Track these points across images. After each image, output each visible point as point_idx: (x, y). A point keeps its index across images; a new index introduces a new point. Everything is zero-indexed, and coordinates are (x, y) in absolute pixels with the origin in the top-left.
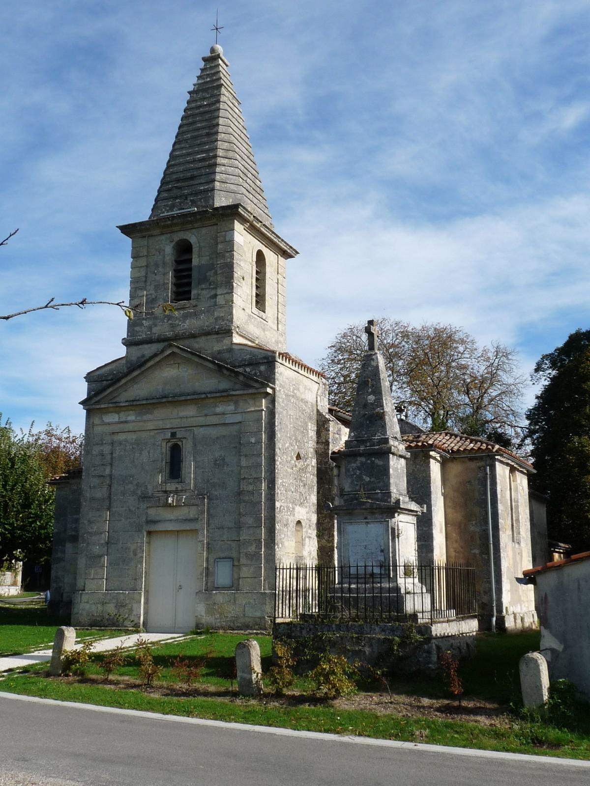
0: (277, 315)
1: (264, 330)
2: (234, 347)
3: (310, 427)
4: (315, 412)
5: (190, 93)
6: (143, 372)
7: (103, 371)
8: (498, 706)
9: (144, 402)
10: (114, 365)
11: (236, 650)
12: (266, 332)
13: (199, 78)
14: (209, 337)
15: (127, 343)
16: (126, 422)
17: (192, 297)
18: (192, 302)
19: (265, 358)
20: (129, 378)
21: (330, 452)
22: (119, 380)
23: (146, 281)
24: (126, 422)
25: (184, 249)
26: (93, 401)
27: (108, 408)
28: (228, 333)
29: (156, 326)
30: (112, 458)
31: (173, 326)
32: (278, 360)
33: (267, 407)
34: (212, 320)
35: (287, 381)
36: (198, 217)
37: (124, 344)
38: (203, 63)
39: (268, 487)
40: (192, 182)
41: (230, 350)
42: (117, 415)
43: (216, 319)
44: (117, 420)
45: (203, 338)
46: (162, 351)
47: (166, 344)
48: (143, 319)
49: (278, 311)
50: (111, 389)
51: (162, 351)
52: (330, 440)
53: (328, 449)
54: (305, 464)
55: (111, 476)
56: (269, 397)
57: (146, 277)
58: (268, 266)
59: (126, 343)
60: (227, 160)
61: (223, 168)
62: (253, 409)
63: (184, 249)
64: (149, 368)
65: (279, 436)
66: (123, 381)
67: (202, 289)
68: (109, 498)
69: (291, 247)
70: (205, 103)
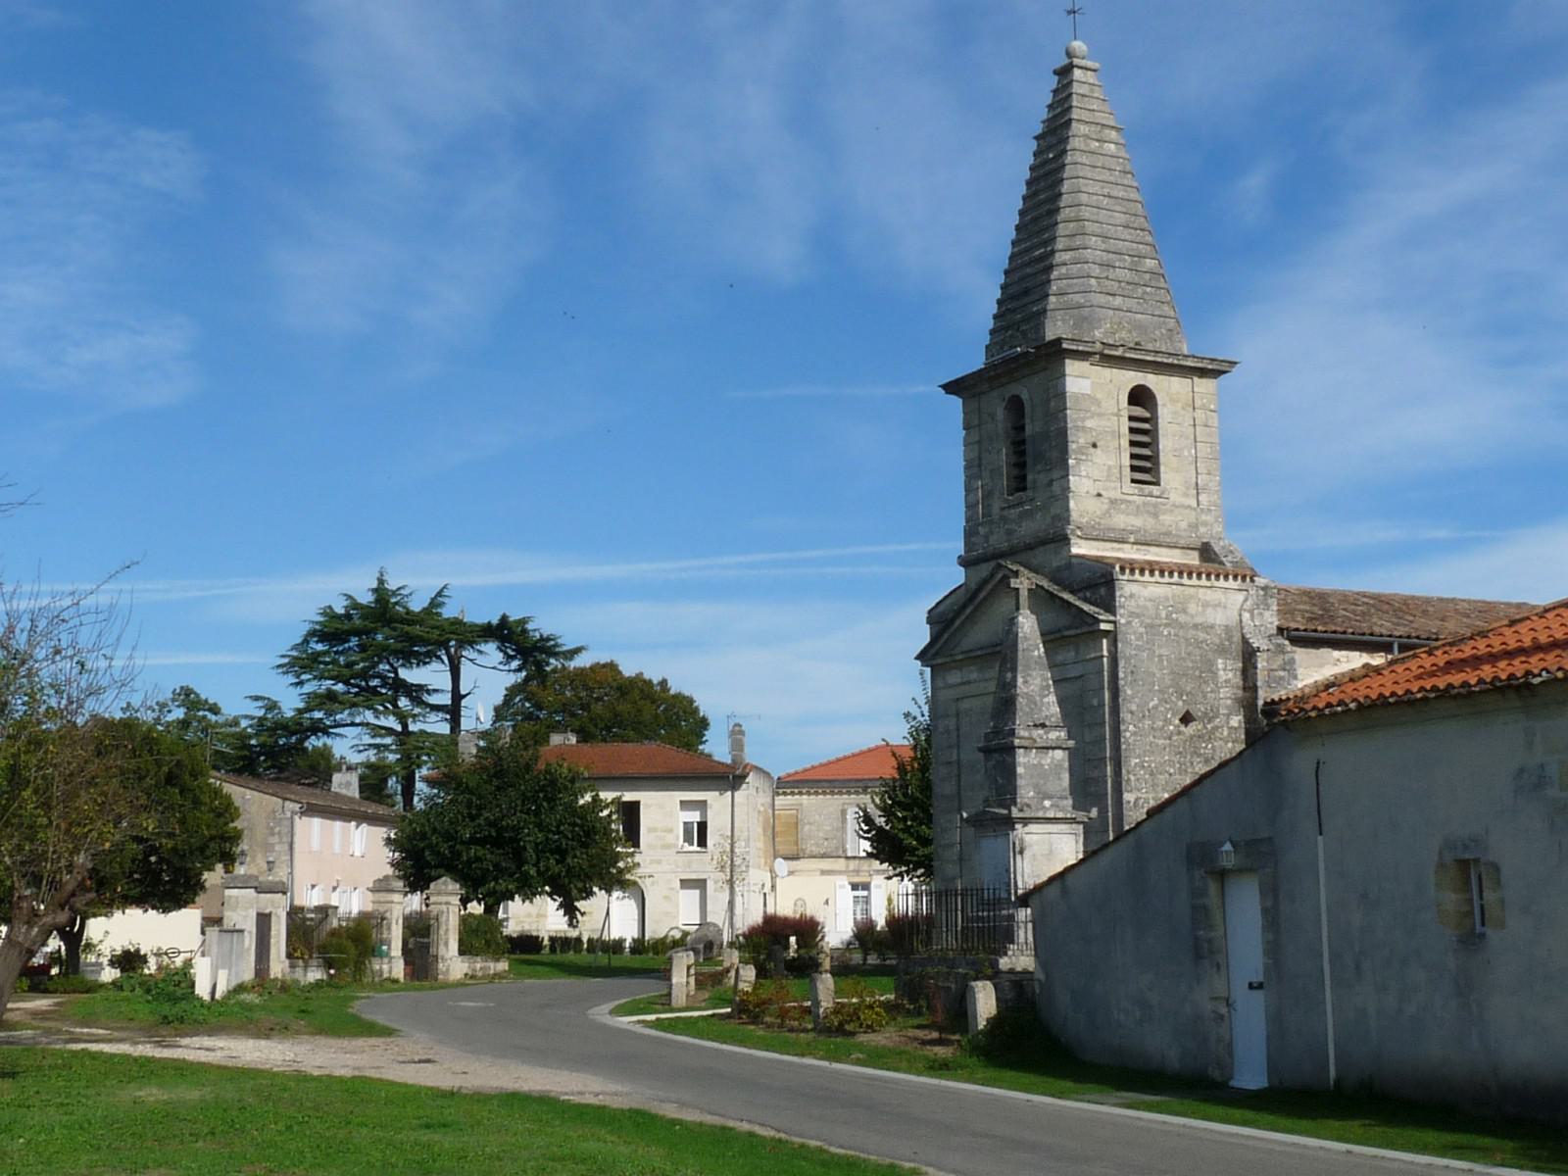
0: (1194, 479)
1: (1155, 515)
2: (1074, 560)
3: (1220, 666)
4: (1237, 638)
5: (1037, 138)
6: (976, 609)
7: (941, 608)
8: (982, 1024)
9: (979, 653)
10: (948, 602)
11: (99, 895)
12: (1161, 517)
13: (1050, 107)
14: (1047, 546)
15: (965, 562)
16: (969, 682)
17: (1029, 485)
18: (1030, 493)
19: (1103, 576)
20: (963, 617)
21: (1260, 703)
22: (953, 620)
23: (980, 466)
24: (969, 682)
25: (1016, 406)
26: (929, 655)
27: (946, 663)
28: (1065, 540)
29: (992, 533)
30: (958, 736)
31: (1009, 533)
32: (1121, 577)
33: (1109, 651)
34: (1048, 520)
35: (1149, 604)
36: (1022, 361)
37: (960, 564)
38: (1056, 78)
39: (1115, 772)
40: (1026, 300)
41: (1069, 566)
42: (959, 674)
43: (1053, 518)
44: (959, 680)
45: (1041, 549)
46: (992, 575)
47: (992, 564)
48: (979, 524)
49: (1197, 473)
50: (946, 636)
51: (992, 575)
52: (1259, 684)
53: (1256, 698)
54: (1209, 726)
55: (958, 762)
56: (1112, 635)
57: (980, 459)
58: (1164, 405)
59: (964, 562)
60: (1070, 253)
61: (1063, 270)
62: (1093, 655)
63: (1016, 406)
64: (985, 599)
65: (1129, 692)
66: (958, 622)
67: (1039, 472)
68: (959, 793)
69: (1213, 360)
70: (1051, 156)
